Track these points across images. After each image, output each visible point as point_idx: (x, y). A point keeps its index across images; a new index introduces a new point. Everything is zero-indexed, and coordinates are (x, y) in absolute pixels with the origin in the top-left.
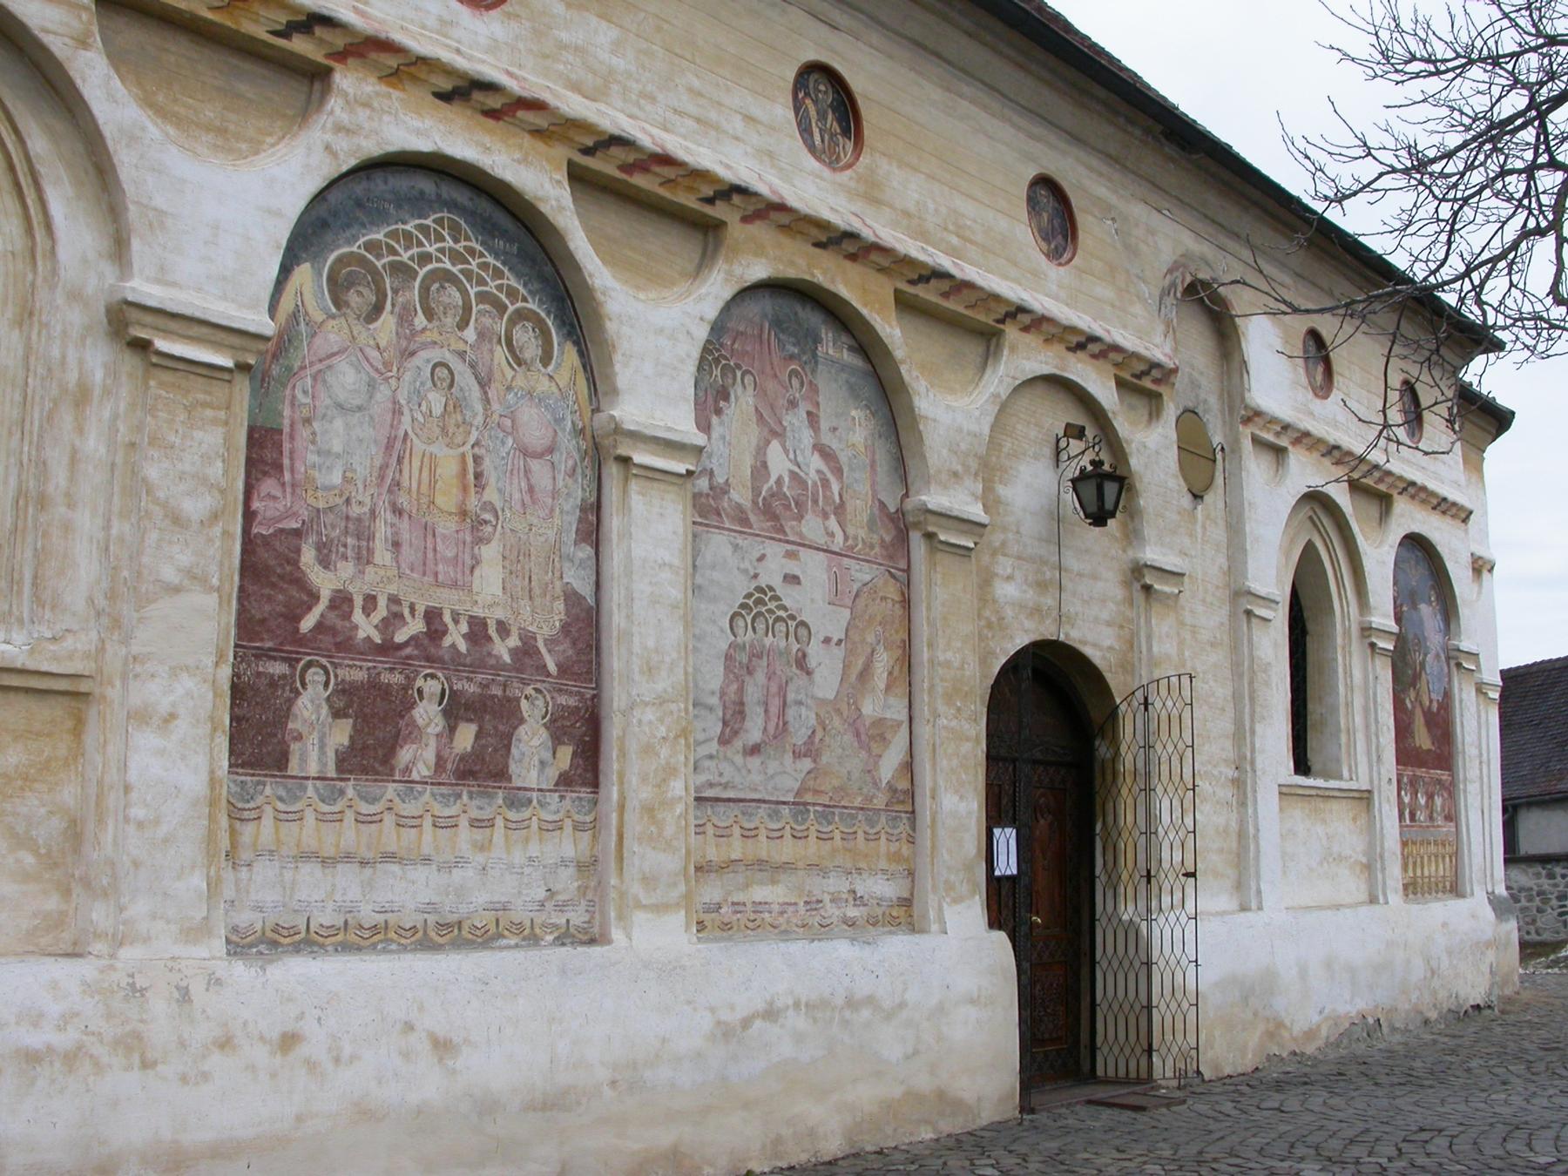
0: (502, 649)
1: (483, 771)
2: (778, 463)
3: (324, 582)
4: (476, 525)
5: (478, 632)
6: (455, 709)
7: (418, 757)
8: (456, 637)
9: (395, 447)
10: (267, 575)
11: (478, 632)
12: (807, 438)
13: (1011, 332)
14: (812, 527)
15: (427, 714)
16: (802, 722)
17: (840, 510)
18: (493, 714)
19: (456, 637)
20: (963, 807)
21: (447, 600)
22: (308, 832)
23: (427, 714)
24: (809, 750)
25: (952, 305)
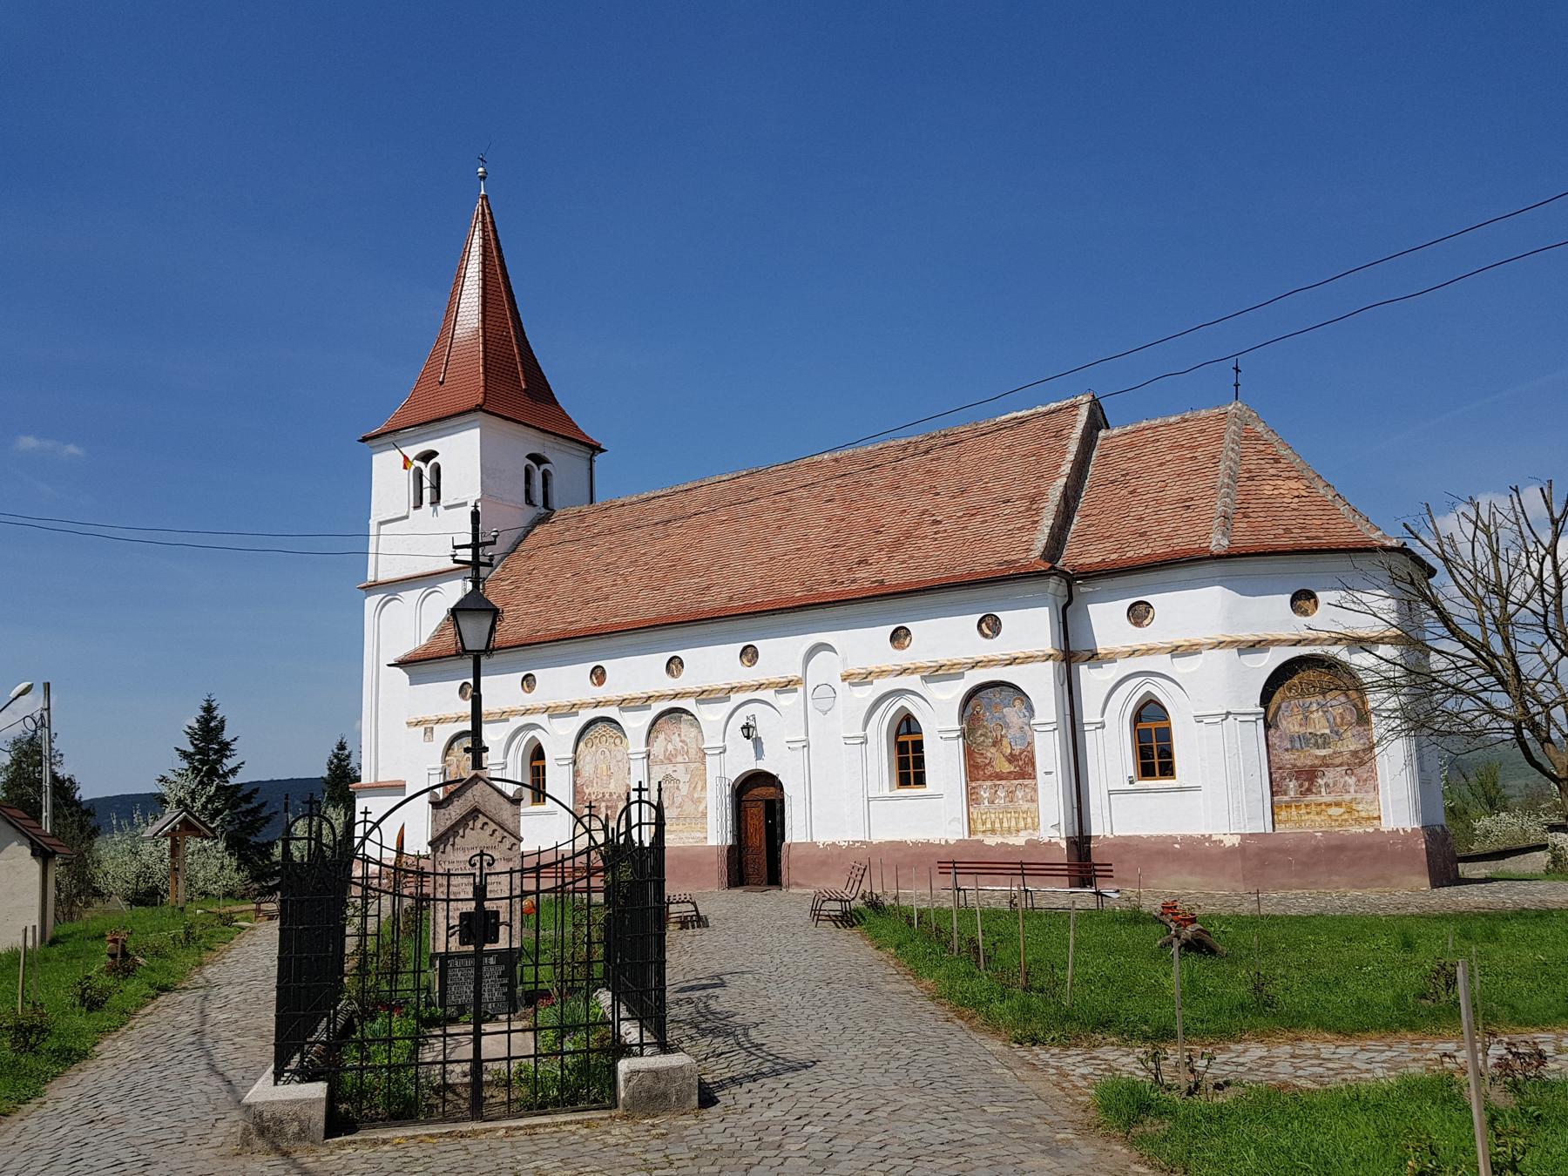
2: (670, 747)
4: (610, 777)
9: (596, 768)
14: (680, 759)
16: (678, 801)
24: (680, 806)
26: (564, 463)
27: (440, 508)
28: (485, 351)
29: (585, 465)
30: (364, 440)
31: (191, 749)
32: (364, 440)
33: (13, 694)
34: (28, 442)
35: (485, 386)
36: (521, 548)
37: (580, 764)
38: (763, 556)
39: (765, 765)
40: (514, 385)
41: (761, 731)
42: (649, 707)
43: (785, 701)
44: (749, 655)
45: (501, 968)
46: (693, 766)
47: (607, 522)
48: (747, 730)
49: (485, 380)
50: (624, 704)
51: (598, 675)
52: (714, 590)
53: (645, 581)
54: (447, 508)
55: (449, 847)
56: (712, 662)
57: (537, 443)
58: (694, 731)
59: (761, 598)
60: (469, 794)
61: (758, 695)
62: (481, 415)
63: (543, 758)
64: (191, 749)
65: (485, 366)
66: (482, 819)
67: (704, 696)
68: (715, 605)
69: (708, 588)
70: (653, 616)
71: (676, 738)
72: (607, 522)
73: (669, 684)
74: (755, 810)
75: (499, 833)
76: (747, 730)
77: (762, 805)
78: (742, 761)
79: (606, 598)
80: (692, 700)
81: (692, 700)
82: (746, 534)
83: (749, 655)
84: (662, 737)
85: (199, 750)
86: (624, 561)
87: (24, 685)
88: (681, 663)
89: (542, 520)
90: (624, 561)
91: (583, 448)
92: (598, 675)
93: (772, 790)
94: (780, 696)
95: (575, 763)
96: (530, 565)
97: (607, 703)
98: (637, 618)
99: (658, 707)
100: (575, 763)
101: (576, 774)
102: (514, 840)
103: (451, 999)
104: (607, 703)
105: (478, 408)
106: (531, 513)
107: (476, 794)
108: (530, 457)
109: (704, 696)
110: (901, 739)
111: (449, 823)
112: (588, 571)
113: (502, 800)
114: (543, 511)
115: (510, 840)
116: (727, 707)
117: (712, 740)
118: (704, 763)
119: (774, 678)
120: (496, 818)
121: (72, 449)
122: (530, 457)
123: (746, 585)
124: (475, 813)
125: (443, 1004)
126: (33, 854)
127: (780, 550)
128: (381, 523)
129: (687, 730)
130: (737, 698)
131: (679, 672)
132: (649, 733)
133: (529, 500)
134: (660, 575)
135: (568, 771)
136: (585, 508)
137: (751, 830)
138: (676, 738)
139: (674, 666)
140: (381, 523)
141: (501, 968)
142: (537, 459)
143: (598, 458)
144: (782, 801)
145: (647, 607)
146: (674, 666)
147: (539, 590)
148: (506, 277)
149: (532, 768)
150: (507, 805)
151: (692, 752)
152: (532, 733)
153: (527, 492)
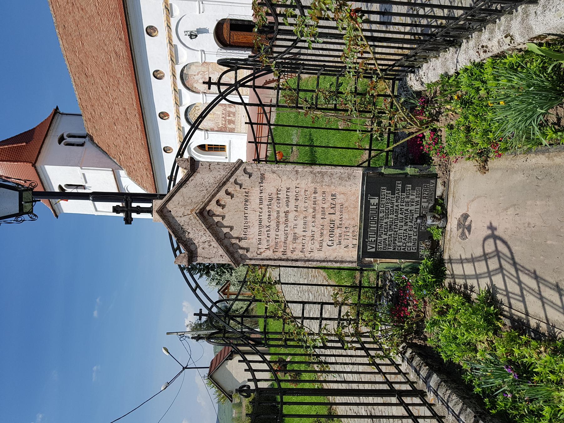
0: (224, 112)
1: (234, 114)
3: (221, 125)
5: (223, 114)
6: (229, 116)
7: (233, 119)
8: (224, 116)
10: (220, 130)
11: (223, 114)
12: (197, 76)
13: (173, 44)
15: (230, 118)
17: (204, 72)
18: (229, 114)
19: (224, 116)
20: (495, 50)
21: (221, 117)
22: (239, 127)
23: (230, 118)
25: (178, 99)
26: (63, 127)
27: (87, 185)
28: (7, 161)
29: (64, 117)
30: (57, 216)
31: (199, 274)
32: (57, 216)
33: (167, 354)
34: (95, 313)
35: (24, 162)
36: (105, 150)
37: (208, 128)
38: (97, 20)
39: (212, 28)
40: (26, 145)
41: (193, 28)
42: (180, 90)
43: (177, 12)
44: (151, 31)
45: (384, 191)
46: (210, 70)
47: (89, 107)
48: (192, 36)
49: (21, 162)
50: (178, 103)
51: (164, 116)
52: (117, 49)
53: (115, 88)
54: (86, 182)
55: (243, 244)
56: (156, 53)
57: (52, 140)
58: (193, 67)
59: (119, 20)
60: (181, 221)
61: (173, 27)
62: (37, 165)
63: (204, 145)
64: (199, 274)
65: (14, 162)
66: (213, 207)
67: (174, 60)
68: (124, 50)
69: (116, 53)
70: (132, 85)
71: (196, 78)
72: (89, 107)
73: (168, 78)
74: (235, 37)
75: (230, 187)
76: (192, 36)
77: (232, 33)
78: (208, 41)
79: (125, 109)
80: (176, 66)
81: (176, 66)
82: (88, 30)
83: (151, 31)
84: (195, 85)
85: (200, 271)
86: (107, 99)
87: (164, 351)
88: (157, 71)
89: (92, 139)
90: (107, 99)
91: (56, 117)
92: (164, 116)
93: (225, 26)
94: (174, 14)
95: (207, 130)
96: (112, 146)
97: (178, 112)
98: (133, 93)
99: (180, 86)
100: (207, 130)
101: (212, 130)
102: (240, 171)
103: (411, 247)
104: (178, 112)
105: (34, 165)
106: (88, 144)
107: (182, 209)
108: (60, 143)
109: (174, 60)
110: (207, 149)
111: (215, 244)
112: (113, 118)
113: (190, 183)
114: (87, 138)
115: (240, 175)
116: (180, 47)
117: (197, 58)
118: (209, 63)
119: (164, 18)
120: (212, 190)
121: (98, 300)
122: (60, 143)
123: (113, 30)
124: (204, 214)
125: (415, 256)
126: (231, 360)
127: (93, 8)
128: (96, 210)
129: (192, 71)
130: (175, 41)
131: (162, 73)
132: (193, 91)
133: (82, 145)
134: (111, 80)
135: (211, 134)
136: (84, 118)
137: (245, 40)
138: (196, 78)
139: (158, 75)
140: (96, 210)
141: (384, 191)
142: (61, 139)
143: (61, 110)
144: (231, 20)
145: (128, 88)
146: (158, 75)
147: (123, 142)
148: (39, 152)
149: (208, 151)
150: (197, 178)
151: (204, 69)
152: (192, 149)
153: (78, 145)
